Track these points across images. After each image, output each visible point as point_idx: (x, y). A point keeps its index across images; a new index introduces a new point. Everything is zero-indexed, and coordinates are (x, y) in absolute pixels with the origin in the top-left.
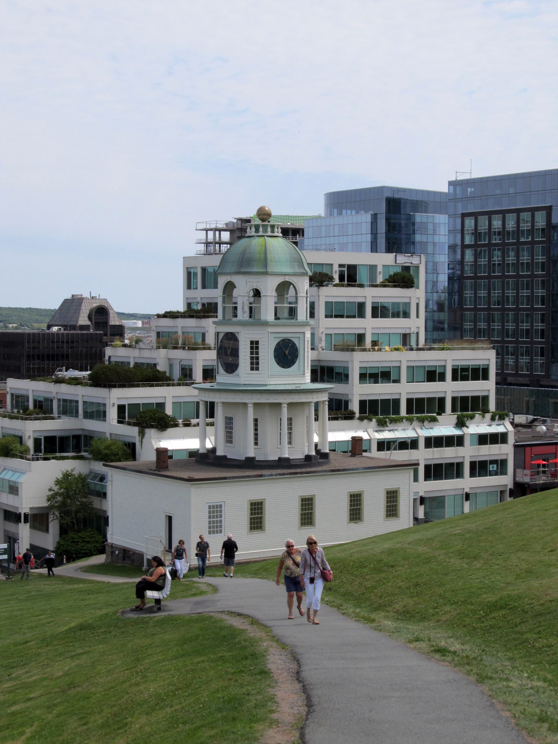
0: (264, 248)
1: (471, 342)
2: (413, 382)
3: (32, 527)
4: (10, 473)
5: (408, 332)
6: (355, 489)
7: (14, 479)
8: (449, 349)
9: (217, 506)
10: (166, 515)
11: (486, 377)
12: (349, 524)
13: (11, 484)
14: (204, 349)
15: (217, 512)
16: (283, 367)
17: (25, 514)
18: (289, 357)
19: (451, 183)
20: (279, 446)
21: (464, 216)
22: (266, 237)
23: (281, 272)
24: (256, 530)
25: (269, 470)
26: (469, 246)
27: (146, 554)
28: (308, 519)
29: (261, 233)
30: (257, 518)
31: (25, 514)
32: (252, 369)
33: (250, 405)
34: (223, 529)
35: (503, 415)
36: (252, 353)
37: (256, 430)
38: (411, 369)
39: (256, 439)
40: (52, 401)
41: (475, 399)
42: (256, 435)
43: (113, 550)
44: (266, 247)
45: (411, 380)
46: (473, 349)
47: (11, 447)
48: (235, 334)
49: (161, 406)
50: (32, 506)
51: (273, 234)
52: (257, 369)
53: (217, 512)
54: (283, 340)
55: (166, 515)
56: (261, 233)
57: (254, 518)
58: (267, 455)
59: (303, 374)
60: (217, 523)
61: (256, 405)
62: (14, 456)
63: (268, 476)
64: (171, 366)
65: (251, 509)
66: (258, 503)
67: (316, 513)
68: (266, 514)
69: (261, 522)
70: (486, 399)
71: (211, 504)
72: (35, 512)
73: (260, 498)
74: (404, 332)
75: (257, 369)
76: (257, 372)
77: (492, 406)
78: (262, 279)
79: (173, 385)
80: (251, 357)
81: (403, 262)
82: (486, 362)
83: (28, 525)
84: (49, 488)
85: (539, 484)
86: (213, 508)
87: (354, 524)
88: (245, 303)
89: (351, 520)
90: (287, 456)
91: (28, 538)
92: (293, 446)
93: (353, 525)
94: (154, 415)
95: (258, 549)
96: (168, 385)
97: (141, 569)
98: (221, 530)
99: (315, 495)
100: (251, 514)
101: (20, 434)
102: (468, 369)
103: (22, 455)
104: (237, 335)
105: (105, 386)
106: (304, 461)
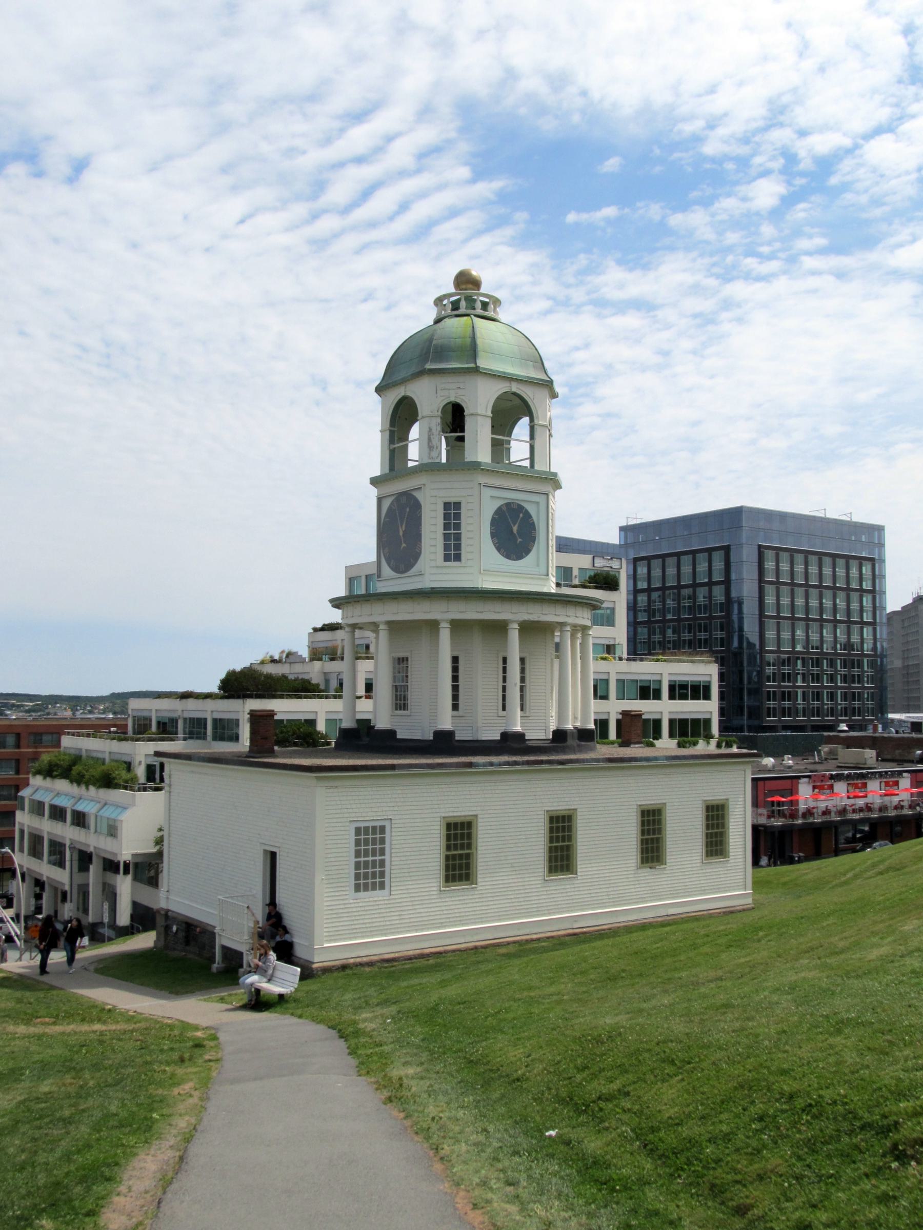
0: (471, 328)
1: (690, 654)
2: (623, 699)
3: (136, 879)
4: (112, 809)
5: (612, 642)
6: (651, 799)
7: (113, 816)
8: (665, 661)
9: (374, 828)
10: (265, 851)
11: (707, 697)
12: (640, 871)
13: (111, 823)
14: (368, 658)
15: (374, 841)
16: (508, 557)
17: (125, 862)
18: (519, 540)
19: (622, 529)
20: (502, 713)
21: (636, 561)
22: (472, 316)
23: (504, 373)
24: (464, 882)
25: (483, 757)
26: (642, 591)
27: (220, 935)
28: (562, 860)
29: (462, 310)
30: (461, 856)
31: (125, 862)
32: (447, 558)
33: (443, 625)
34: (387, 880)
35: (730, 741)
36: (446, 526)
37: (455, 678)
38: (621, 683)
39: (455, 697)
40: (177, 721)
41: (696, 722)
42: (455, 688)
43: (169, 922)
44: (473, 327)
45: (621, 696)
46: (692, 662)
47: (114, 775)
48: (415, 494)
49: (312, 723)
50: (134, 852)
51: (486, 314)
52: (458, 558)
53: (374, 841)
54: (508, 505)
55: (265, 851)
56: (462, 310)
57: (454, 856)
58: (477, 730)
59: (545, 573)
60: (366, 851)
61: (458, 626)
62: (117, 786)
63: (484, 765)
64: (327, 681)
65: (448, 837)
66: (462, 824)
67: (579, 848)
68: (479, 848)
69: (468, 866)
70: (707, 722)
71: (362, 825)
72: (139, 860)
73: (466, 813)
74: (608, 643)
75: (458, 558)
76: (457, 563)
77: (715, 729)
78: (469, 381)
79: (327, 697)
80: (444, 534)
81: (602, 565)
82: (707, 679)
83: (129, 877)
84: (159, 827)
85: (778, 826)
86: (366, 833)
87: (649, 870)
88: (434, 431)
89: (642, 862)
90: (518, 728)
91: (129, 896)
92: (527, 714)
93: (647, 874)
94: (299, 729)
95: (463, 925)
96: (321, 697)
97: (210, 968)
98: (384, 882)
99: (575, 810)
100: (448, 848)
101: (127, 759)
102: (687, 685)
103: (129, 784)
104: (416, 494)
105: (238, 697)
106: (551, 743)
